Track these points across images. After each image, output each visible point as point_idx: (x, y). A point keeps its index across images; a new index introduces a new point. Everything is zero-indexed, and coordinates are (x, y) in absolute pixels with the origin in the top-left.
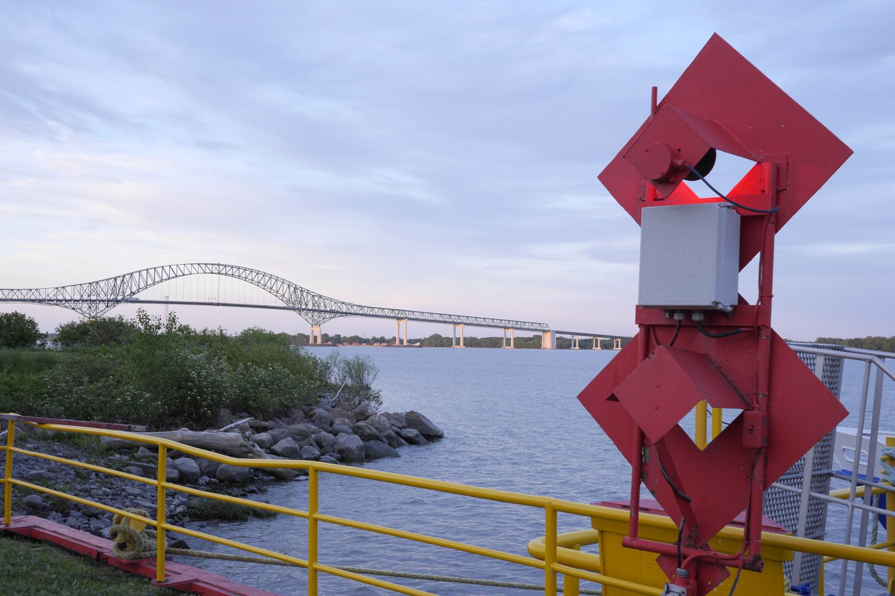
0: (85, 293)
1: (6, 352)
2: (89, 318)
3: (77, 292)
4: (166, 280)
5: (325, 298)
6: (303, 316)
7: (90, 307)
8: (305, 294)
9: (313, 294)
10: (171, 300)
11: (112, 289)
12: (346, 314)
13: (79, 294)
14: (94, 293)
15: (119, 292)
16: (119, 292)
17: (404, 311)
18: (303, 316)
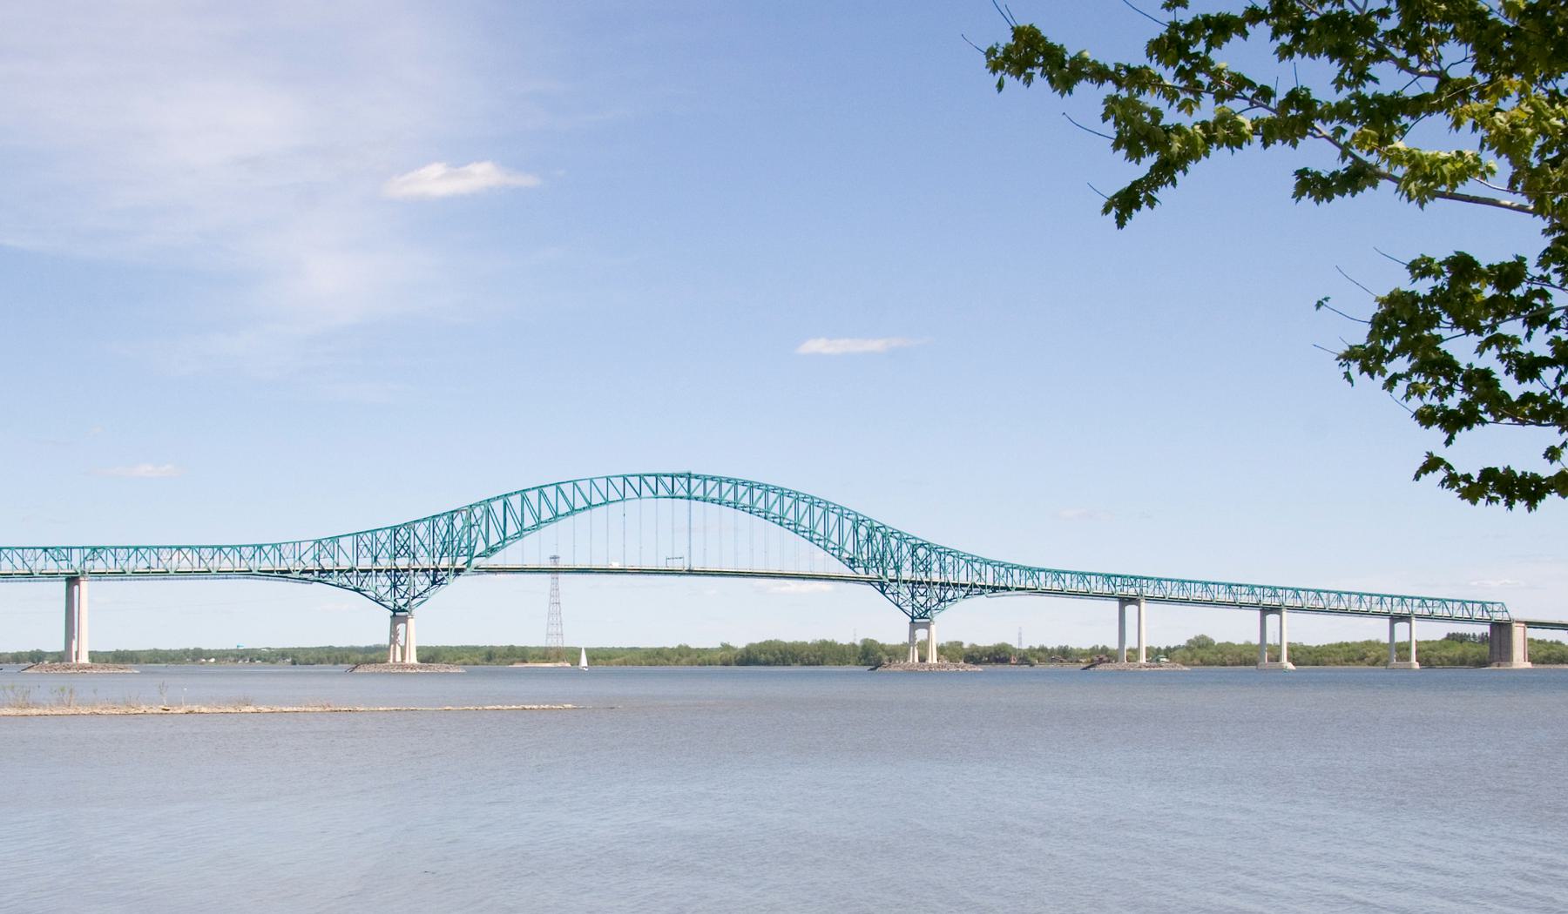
0: (383, 551)
1: (1562, 859)
2: (394, 611)
3: (365, 550)
4: (549, 521)
5: (942, 550)
6: (889, 596)
7: (395, 586)
8: (893, 542)
9: (913, 541)
10: (562, 564)
11: (444, 539)
12: (995, 589)
13: (369, 555)
14: (402, 552)
15: (459, 548)
16: (459, 548)
17: (1136, 578)
18: (890, 596)
